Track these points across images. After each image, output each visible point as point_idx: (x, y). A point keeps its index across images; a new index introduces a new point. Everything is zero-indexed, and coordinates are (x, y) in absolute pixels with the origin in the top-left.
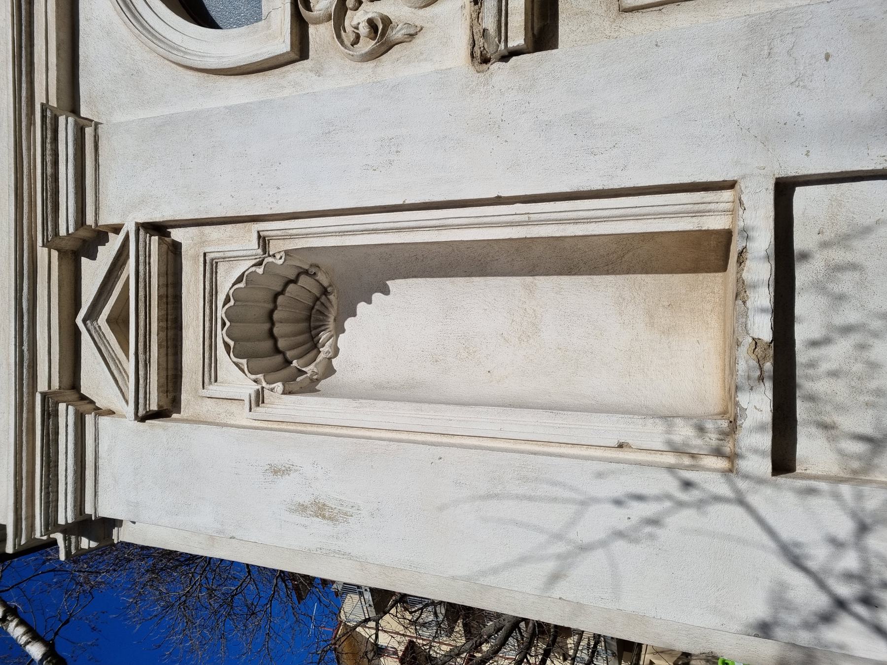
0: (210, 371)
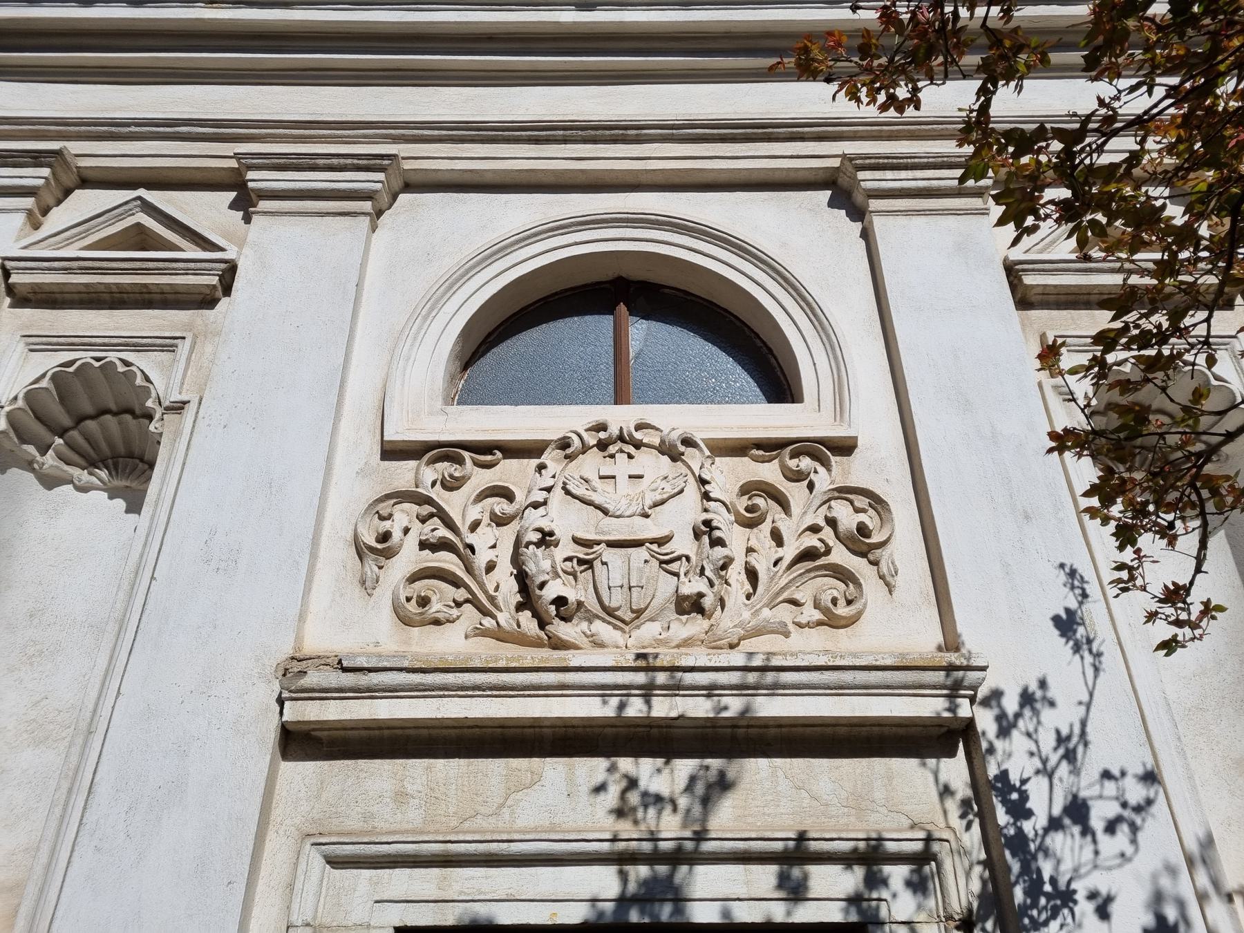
0: (39, 344)
